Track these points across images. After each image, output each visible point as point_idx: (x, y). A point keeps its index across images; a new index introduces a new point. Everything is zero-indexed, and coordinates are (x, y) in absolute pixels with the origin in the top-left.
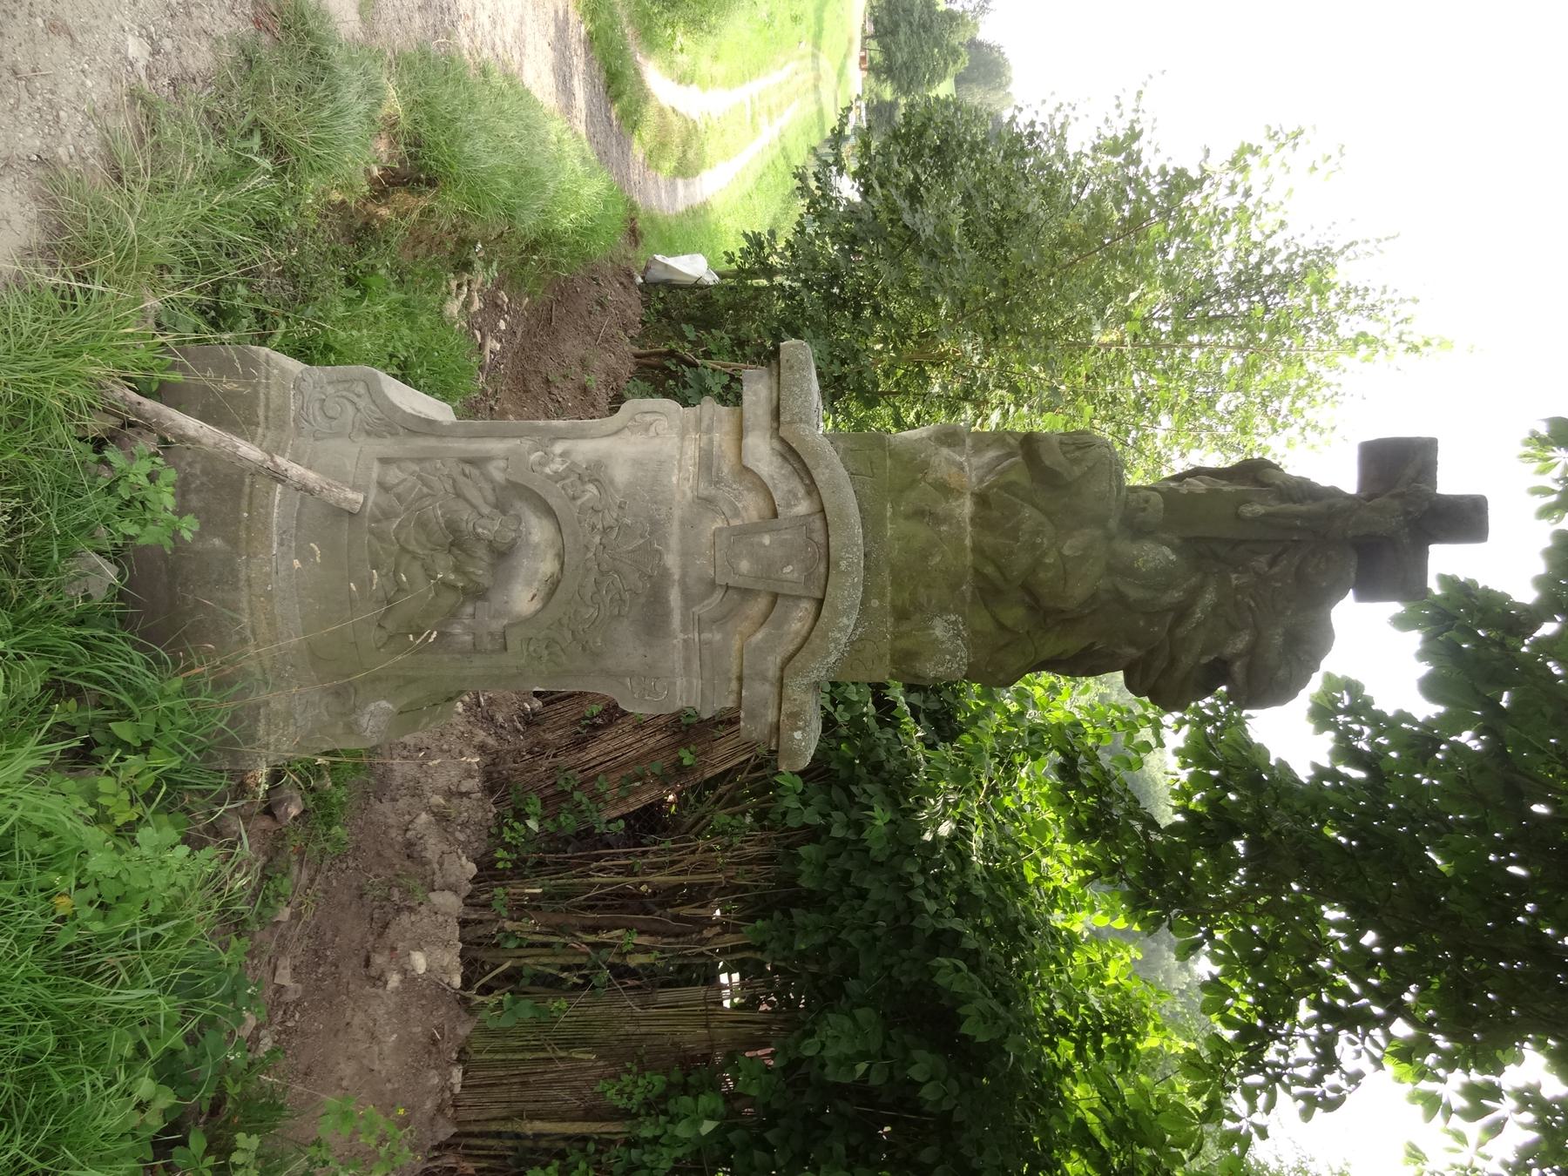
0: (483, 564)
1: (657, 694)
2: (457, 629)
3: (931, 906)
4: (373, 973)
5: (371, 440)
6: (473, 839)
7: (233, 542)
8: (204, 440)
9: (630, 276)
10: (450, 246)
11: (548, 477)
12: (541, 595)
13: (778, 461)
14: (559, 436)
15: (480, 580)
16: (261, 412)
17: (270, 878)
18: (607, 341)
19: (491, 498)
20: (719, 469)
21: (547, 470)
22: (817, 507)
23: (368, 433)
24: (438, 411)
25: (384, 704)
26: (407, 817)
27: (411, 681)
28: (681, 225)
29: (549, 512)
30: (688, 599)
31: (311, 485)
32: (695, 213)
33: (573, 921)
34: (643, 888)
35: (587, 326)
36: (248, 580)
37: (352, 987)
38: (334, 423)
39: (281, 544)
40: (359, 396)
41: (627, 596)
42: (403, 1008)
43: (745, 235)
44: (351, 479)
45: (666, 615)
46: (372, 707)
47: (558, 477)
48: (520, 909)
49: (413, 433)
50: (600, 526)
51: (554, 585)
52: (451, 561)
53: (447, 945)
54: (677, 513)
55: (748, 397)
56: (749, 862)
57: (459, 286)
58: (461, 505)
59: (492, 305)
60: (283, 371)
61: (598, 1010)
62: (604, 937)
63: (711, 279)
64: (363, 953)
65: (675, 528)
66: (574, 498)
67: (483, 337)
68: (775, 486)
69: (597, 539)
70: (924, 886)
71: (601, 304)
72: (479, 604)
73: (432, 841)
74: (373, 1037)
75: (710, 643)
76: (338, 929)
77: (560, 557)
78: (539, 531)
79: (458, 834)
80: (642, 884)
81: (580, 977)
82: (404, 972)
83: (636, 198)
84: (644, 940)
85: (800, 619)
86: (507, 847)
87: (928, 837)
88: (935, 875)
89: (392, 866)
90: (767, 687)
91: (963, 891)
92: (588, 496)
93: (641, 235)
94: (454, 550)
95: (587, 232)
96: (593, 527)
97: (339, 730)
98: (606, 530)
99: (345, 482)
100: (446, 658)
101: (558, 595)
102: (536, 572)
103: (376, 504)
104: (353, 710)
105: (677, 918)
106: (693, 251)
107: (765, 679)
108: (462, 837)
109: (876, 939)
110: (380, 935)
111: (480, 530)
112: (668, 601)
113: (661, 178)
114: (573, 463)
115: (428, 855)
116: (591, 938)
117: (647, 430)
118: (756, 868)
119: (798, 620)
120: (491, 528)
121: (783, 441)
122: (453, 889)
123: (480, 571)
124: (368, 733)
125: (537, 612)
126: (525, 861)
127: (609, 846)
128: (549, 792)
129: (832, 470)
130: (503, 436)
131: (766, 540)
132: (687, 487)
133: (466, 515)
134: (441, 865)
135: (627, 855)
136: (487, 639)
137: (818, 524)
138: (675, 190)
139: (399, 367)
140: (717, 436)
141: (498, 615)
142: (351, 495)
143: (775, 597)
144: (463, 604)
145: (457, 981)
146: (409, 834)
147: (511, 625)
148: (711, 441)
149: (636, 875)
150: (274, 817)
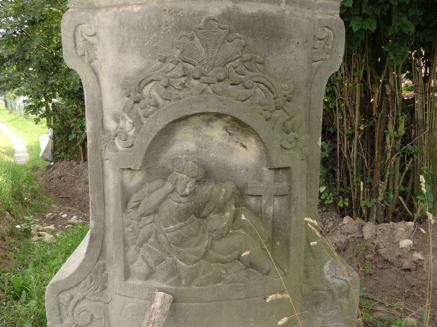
0: (216, 189)
2: (270, 210)
4: (414, 267)
5: (110, 285)
6: (331, 219)
9: (49, 167)
11: (137, 131)
14: (101, 126)
15: (230, 190)
18: (78, 173)
19: (157, 183)
23: (104, 288)
25: (326, 268)
28: (34, 154)
29: (168, 131)
32: (30, 150)
33: (379, 164)
34: (362, 128)
35: (71, 182)
37: (424, 278)
38: (96, 316)
40: (72, 297)
41: (246, 56)
44: (143, 302)
45: (264, 18)
46: (328, 277)
47: (138, 123)
48: (372, 192)
49: (102, 252)
51: (238, 126)
52: (214, 216)
53: (393, 229)
56: (350, 70)
57: (39, 235)
58: (165, 209)
59: (53, 220)
61: (425, 151)
62: (389, 147)
63: (50, 132)
66: (157, 106)
69: (195, 83)
76: (391, 286)
78: (185, 142)
80: (359, 130)
81: (408, 159)
82: (412, 251)
84: (391, 128)
92: (154, 93)
93: (35, 166)
96: (183, 86)
99: (146, 309)
100: (293, 219)
101: (245, 118)
102: (222, 144)
103: (165, 280)
104: (330, 291)
108: (330, 225)
110: (391, 263)
111: (187, 191)
112: (252, 16)
114: (124, 110)
115: (343, 240)
116: (389, 155)
117: (92, 45)
118: (353, 67)
123: (224, 191)
124: (349, 279)
125: (260, 140)
127: (335, 150)
130: (103, 175)
133: (173, 204)
134: (348, 234)
135: (342, 139)
136: (279, 185)
142: (158, 303)
144: (247, 206)
147: (269, 161)
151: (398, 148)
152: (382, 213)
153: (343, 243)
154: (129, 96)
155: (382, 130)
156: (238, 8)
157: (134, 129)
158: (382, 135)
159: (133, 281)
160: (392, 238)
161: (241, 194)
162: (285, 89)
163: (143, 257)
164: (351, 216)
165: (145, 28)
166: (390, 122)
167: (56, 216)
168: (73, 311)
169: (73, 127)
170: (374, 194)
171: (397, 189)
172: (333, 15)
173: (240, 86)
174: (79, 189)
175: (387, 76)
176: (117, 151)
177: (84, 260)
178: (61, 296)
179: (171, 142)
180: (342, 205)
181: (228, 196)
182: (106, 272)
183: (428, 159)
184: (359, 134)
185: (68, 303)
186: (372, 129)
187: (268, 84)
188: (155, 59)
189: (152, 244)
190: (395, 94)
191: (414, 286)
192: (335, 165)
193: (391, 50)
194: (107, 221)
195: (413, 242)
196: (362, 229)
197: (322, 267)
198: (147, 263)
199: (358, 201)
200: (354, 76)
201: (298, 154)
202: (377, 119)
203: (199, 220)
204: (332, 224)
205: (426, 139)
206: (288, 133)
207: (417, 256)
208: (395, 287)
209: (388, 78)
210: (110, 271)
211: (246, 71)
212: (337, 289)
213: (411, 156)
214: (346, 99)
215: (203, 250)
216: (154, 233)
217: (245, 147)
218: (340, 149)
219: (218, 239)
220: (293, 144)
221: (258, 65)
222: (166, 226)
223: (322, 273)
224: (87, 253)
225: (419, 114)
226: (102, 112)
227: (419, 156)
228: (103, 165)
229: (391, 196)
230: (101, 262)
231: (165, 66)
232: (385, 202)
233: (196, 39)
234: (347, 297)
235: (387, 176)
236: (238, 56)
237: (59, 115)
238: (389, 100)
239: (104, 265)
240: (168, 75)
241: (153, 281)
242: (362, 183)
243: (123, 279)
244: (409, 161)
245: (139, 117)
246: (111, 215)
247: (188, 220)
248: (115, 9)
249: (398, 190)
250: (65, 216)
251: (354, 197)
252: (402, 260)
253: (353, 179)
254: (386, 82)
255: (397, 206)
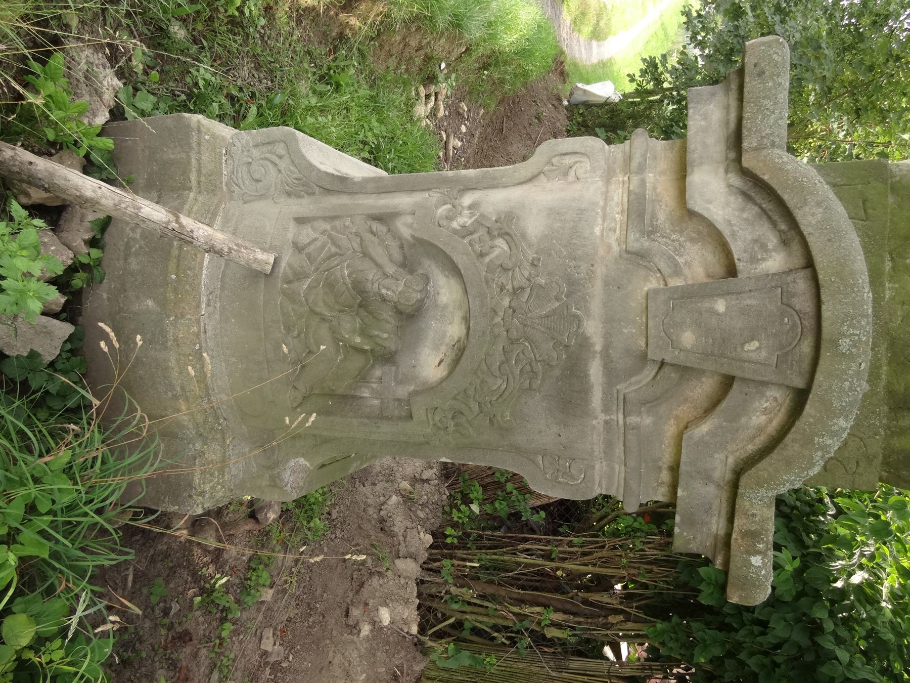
1: (573, 478)
3: (843, 655)
4: (351, 623)
5: (291, 201)
6: (430, 516)
7: (162, 303)
8: (103, 201)
9: (559, 100)
10: (418, 61)
11: (455, 231)
12: (448, 360)
13: (737, 201)
15: (387, 344)
16: (193, 177)
17: (254, 570)
19: (397, 255)
20: (654, 216)
21: (455, 225)
22: (798, 260)
23: (289, 194)
24: (354, 168)
25: (302, 461)
26: (382, 498)
27: (326, 441)
29: (455, 270)
30: (611, 375)
31: (218, 246)
33: (503, 593)
34: (559, 573)
36: (176, 340)
37: (334, 633)
39: (208, 305)
40: (280, 157)
41: (539, 367)
42: (372, 652)
43: (644, 60)
45: (585, 391)
46: (292, 463)
47: (466, 232)
48: (462, 579)
49: (328, 191)
50: (509, 287)
51: (460, 351)
53: (407, 602)
54: (600, 271)
55: (695, 121)
56: (650, 563)
57: (428, 97)
58: (367, 264)
59: (456, 114)
60: (214, 136)
61: (521, 665)
62: (527, 610)
63: (616, 98)
64: (344, 606)
65: (597, 289)
66: (482, 255)
67: (448, 137)
68: (733, 234)
69: (506, 302)
70: (834, 633)
71: (539, 119)
72: (386, 368)
73: (399, 519)
74: (348, 675)
75: (637, 428)
76: (326, 586)
77: (466, 319)
78: (446, 291)
79: (419, 512)
80: (558, 569)
81: (508, 638)
82: (374, 623)
83: (565, 49)
84: (558, 617)
85: (765, 411)
86: (455, 525)
87: (839, 584)
88: (843, 618)
89: (369, 536)
90: (711, 489)
91: (871, 634)
93: (568, 75)
94: (363, 313)
95: (523, 53)
97: (265, 482)
98: (516, 292)
100: (355, 422)
102: (444, 336)
103: (290, 265)
104: (277, 464)
105: (585, 602)
106: (604, 80)
107: (708, 478)
108: (422, 515)
109: (776, 665)
110: (357, 592)
111: (384, 291)
112: (587, 376)
113: (583, 38)
114: (483, 216)
115: (396, 529)
116: (516, 609)
117: (566, 174)
118: (655, 569)
119: (763, 413)
120: (396, 287)
121: (745, 173)
122: (413, 557)
123: (385, 336)
124: (289, 488)
125: (443, 380)
126: (468, 535)
127: (533, 531)
128: (489, 480)
129: (825, 212)
130: (412, 190)
131: (721, 306)
132: (612, 239)
134: (405, 537)
137: (801, 284)
138: (591, 48)
139: (371, 152)
140: (650, 177)
141: (402, 381)
142: (260, 256)
143: (728, 382)
144: (373, 366)
145: (414, 629)
146: (382, 513)
147: (415, 393)
148: (643, 182)
149: (552, 560)
150: (257, 521)
151: (526, 623)
152: (434, 590)
153: (392, 529)
154: (496, 221)
155: (554, 603)
156: (594, 357)
157: (459, 228)
158: (547, 602)
159: (292, 227)
160: (393, 598)
161: (388, 358)
162: (502, 416)
163: (315, 240)
164: (431, 547)
165: (574, 241)
166: (566, 617)
167: (463, 117)
168: (266, 159)
169: (617, 134)
170: (461, 581)
171: (468, 617)
172: (600, 485)
173: (503, 358)
174: (515, 146)
175: (637, 620)
176: (437, 207)
177: (319, 170)
178: (282, 144)
179: (447, 273)
180: (447, 533)
181: (380, 342)
182: (306, 196)
183: (508, 669)
184: (552, 569)
185: (275, 153)
186: (558, 589)
187: (507, 393)
188: (536, 253)
189: (329, 249)
190: (608, 629)
191: (324, 617)
192: (509, 529)
193: (673, 628)
194: (361, 196)
195: (385, 627)
196: (411, 557)
197: (303, 456)
198: (309, 244)
199: (451, 557)
200: (639, 568)
201: (429, 430)
202: (572, 598)
203: (356, 306)
204: (422, 516)
205: (538, 669)
206: (453, 418)
207: (366, 630)
208: (325, 592)
209: (634, 622)
210: (306, 201)
211: (520, 367)
212: (278, 473)
213: (513, 642)
214: (604, 553)
215: (318, 310)
216: (341, 252)
217: (439, 364)
218: (533, 539)
219: (330, 328)
220: (439, 425)
221: (528, 381)
222: (348, 266)
223: (297, 455)
224: (326, 173)
225: (576, 663)
226: (485, 188)
227: (513, 656)
228: (423, 190)
229: (455, 606)
230: (317, 190)
231: (527, 265)
232: (448, 596)
233: (557, 304)
234: (270, 486)
235: (486, 604)
236: (537, 356)
237: (645, 109)
238: (600, 619)
239: (314, 194)
240: (517, 269)
241: (291, 251)
242: (477, 565)
243: (296, 216)
244: (506, 639)
245: (471, 233)
246: (365, 202)
247: (354, 293)
248: (602, 203)
249: (466, 619)
250: (463, 129)
251: (459, 553)
252: (361, 607)
253: (486, 554)
254: (628, 618)
255: (443, 615)
